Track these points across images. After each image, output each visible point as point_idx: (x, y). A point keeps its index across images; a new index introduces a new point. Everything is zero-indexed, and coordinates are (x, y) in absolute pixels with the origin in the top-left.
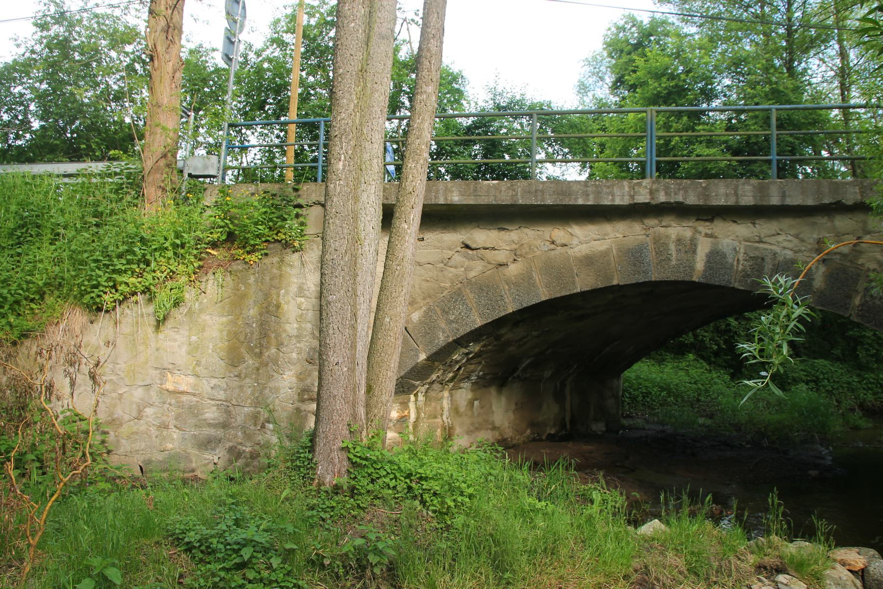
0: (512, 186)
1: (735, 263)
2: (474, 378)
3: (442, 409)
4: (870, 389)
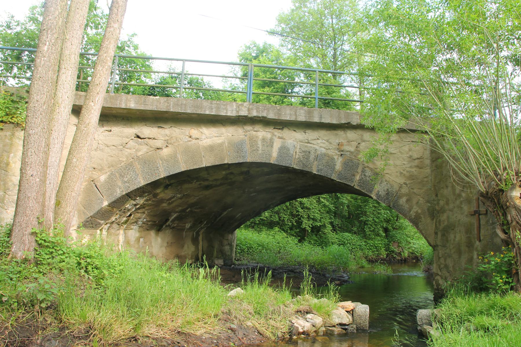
0: (167, 100)
1: (294, 154)
2: (140, 223)
3: (118, 241)
4: (370, 249)
